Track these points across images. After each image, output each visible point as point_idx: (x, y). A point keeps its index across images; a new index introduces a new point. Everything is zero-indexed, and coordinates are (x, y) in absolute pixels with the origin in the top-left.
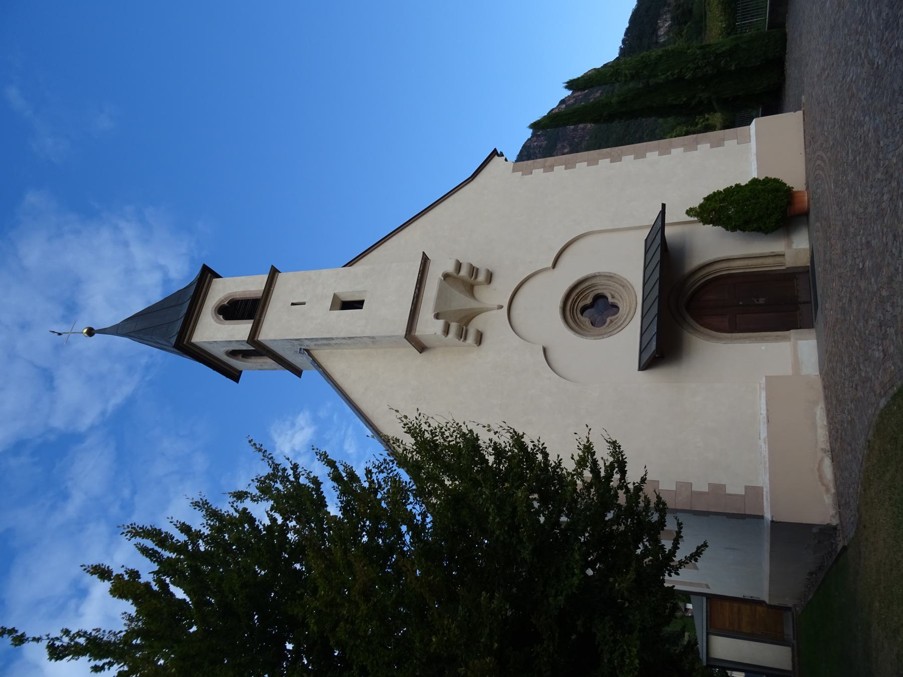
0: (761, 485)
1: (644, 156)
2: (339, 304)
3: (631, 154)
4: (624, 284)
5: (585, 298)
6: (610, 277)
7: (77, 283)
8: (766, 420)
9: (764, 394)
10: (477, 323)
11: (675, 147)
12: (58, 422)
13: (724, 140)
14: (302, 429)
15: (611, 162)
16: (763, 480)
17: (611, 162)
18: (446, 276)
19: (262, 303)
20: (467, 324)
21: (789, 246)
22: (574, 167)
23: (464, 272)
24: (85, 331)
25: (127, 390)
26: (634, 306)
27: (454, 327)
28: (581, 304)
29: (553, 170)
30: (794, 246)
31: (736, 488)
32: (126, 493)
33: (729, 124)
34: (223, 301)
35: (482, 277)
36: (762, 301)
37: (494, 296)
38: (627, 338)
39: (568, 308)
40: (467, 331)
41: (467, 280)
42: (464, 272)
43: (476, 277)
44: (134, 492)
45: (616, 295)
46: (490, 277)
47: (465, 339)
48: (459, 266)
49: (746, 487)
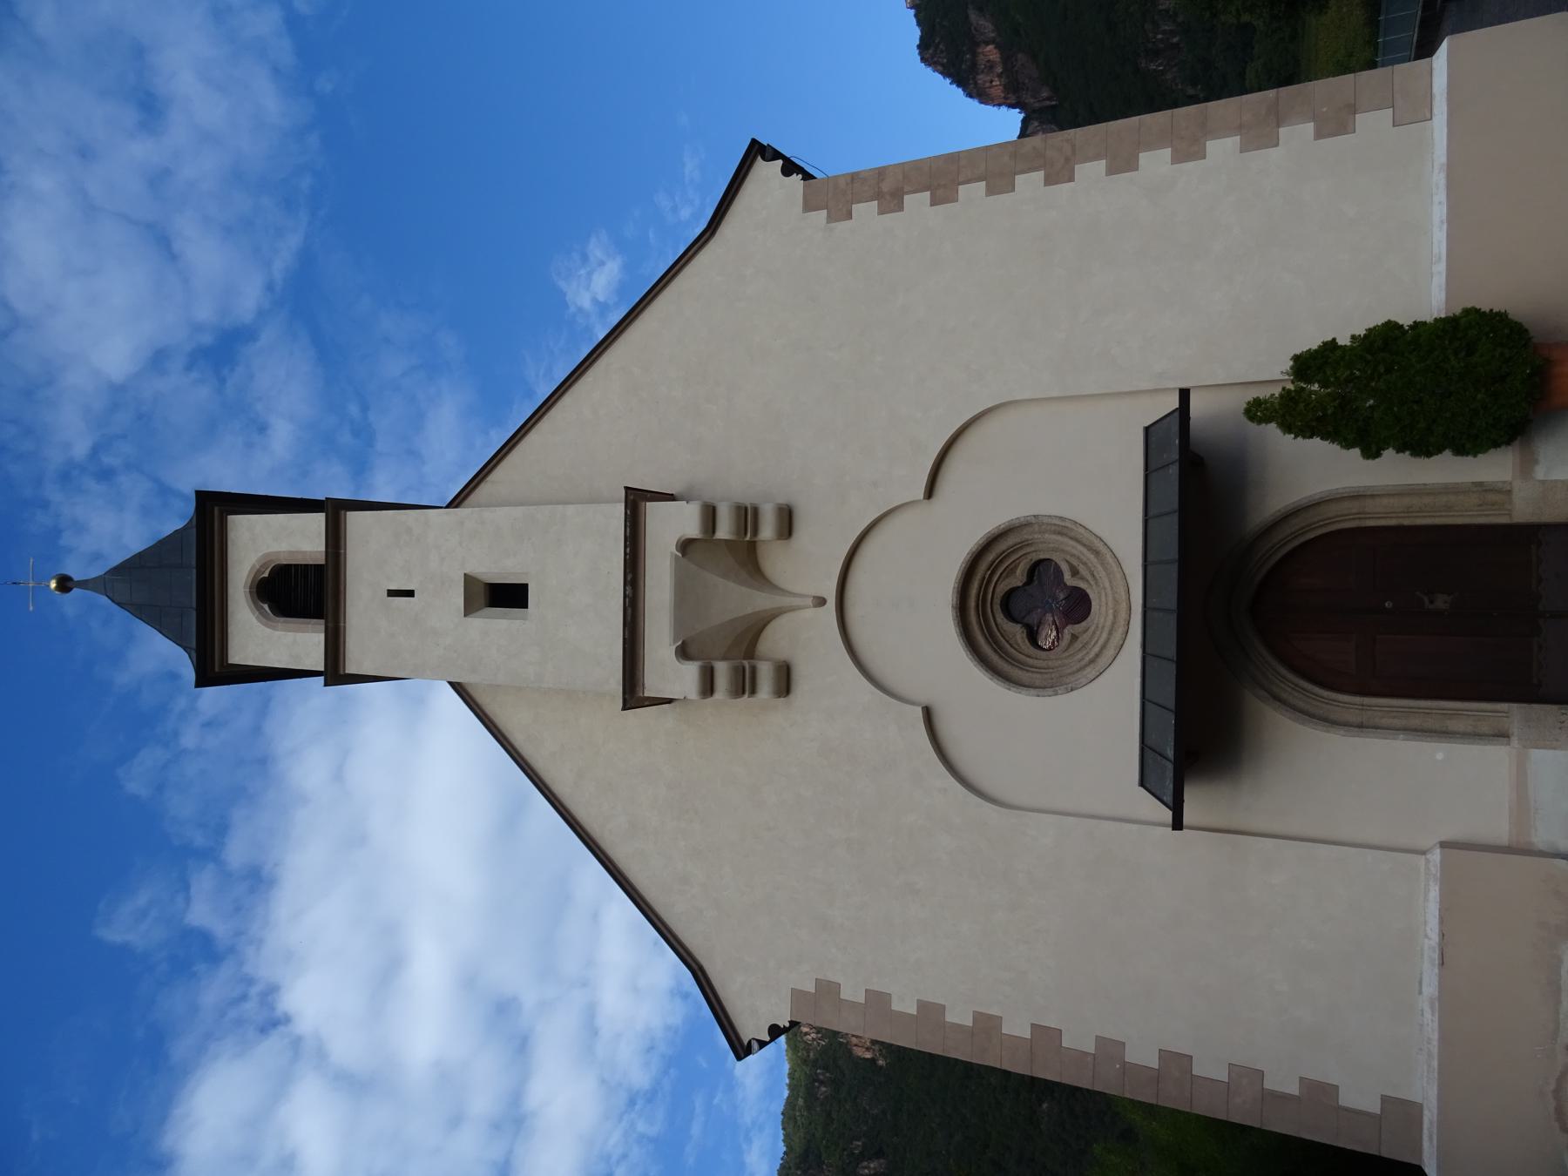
0: (1419, 1100)
1: (1131, 165)
2: (481, 597)
3: (1097, 157)
4: (1097, 547)
5: (1010, 571)
6: (1063, 528)
7: (139, 52)
8: (1436, 956)
9: (1434, 892)
10: (775, 642)
11: (1217, 134)
12: (205, 312)
13: (1353, 109)
14: (602, 264)
15: (1048, 181)
16: (1424, 1090)
17: (1048, 181)
18: (686, 546)
19: (330, 573)
20: (751, 653)
21: (1527, 466)
22: (953, 199)
23: (724, 531)
24: (53, 585)
25: (293, 241)
26: (1123, 615)
27: (722, 670)
28: (1003, 588)
29: (900, 207)
30: (1540, 473)
31: (1360, 1096)
32: (354, 409)
33: (1366, 54)
34: (259, 572)
35: (767, 530)
36: (1441, 602)
37: (804, 567)
38: (1105, 705)
39: (972, 603)
40: (754, 671)
41: (739, 541)
42: (724, 531)
43: (755, 531)
44: (365, 408)
45: (1083, 571)
46: (787, 521)
47: (753, 692)
48: (710, 515)
49: (1385, 1100)
